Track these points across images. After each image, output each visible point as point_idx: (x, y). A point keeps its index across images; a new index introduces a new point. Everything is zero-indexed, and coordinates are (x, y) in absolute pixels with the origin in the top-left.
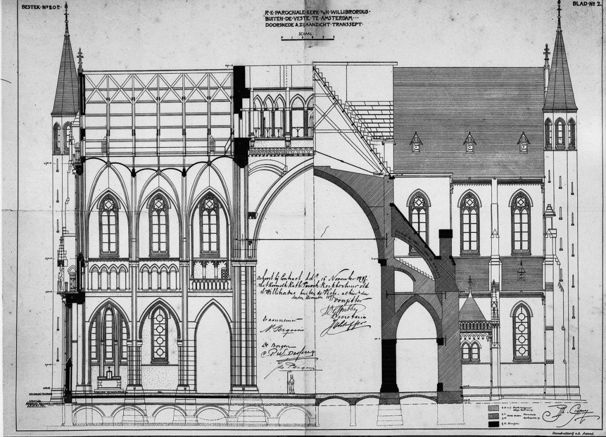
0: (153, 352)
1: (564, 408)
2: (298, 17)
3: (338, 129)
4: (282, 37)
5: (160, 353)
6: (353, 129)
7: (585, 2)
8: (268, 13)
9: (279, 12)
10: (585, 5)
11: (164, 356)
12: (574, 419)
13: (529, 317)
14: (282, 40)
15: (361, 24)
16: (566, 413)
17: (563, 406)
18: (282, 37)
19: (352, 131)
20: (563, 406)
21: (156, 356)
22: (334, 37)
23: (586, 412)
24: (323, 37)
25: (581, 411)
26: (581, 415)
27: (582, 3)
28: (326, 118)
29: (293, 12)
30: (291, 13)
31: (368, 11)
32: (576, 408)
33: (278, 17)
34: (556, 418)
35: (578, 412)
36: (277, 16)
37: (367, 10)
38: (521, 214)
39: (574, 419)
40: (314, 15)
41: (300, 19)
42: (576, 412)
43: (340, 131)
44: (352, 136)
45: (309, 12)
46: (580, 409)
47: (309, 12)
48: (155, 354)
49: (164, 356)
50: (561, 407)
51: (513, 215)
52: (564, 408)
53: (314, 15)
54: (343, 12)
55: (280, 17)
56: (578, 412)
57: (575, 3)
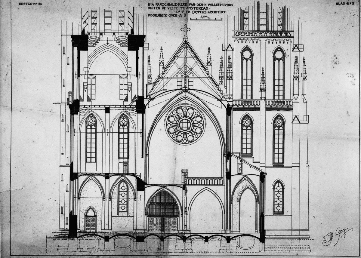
0: (274, 208)
1: (332, 234)
2: (170, 7)
3: (199, 77)
4: (191, 18)
5: (278, 209)
6: (207, 77)
7: (343, 3)
8: (150, 5)
9: (158, 4)
10: (343, 4)
11: (281, 210)
12: (340, 237)
13: (283, 188)
14: (190, 20)
15: (225, 12)
16: (334, 236)
17: (331, 233)
18: (191, 18)
19: (198, 78)
20: (331, 233)
21: (276, 210)
22: (222, 18)
23: (345, 230)
24: (216, 19)
25: (342, 231)
26: (343, 233)
27: (342, 3)
28: (192, 70)
29: (167, 4)
30: (166, 4)
31: (233, 5)
32: (338, 231)
33: (157, 7)
34: (330, 242)
35: (340, 232)
36: (157, 6)
37: (232, 4)
38: (247, 130)
39: (340, 237)
40: (182, 6)
41: (171, 8)
42: (339, 233)
43: (200, 78)
44: (207, 81)
45: (180, 4)
46: (341, 230)
47: (180, 4)
48: (276, 209)
49: (281, 210)
50: (330, 234)
51: (242, 129)
52: (332, 234)
53: (182, 6)
54: (216, 5)
55: (158, 7)
56: (340, 232)
57: (337, 4)
